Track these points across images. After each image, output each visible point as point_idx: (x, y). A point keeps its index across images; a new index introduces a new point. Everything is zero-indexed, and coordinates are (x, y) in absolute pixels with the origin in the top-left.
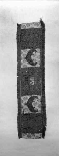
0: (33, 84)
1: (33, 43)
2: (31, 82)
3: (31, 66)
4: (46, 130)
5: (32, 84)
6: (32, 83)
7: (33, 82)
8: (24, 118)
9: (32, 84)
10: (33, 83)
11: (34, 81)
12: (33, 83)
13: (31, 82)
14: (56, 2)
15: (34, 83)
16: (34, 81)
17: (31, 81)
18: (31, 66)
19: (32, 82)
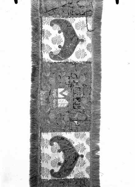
0: (60, 90)
5: (64, 91)
7: (60, 96)
9: (64, 91)
10: (61, 93)
11: (57, 98)
12: (61, 93)
13: (66, 96)
16: (57, 98)
17: (65, 97)
19: (64, 95)
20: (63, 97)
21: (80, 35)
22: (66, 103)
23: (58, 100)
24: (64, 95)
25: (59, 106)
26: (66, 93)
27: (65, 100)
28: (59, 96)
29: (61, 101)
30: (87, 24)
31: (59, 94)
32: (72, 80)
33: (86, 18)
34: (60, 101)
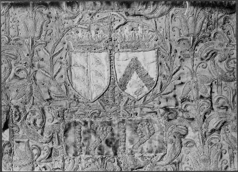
0: (148, 60)
1: (110, 102)
2: (131, 90)
3: (3, 145)
4: (105, 143)
5: (144, 76)
6: (135, 76)
7: (123, 61)
8: (134, 100)
9: (144, 76)
10: (135, 66)
11: (111, 47)
12: (135, 66)
13: (123, 86)
14: (1, 6)
15: (136, 46)
16: (111, 47)
17: (116, 85)
18: (3, 145)
19: (127, 76)
20: (119, 76)
21: (225, 29)
22: (92, 88)
23: (104, 56)
24: (127, 76)
25: (78, 58)
26: (134, 87)
27: (105, 84)
28: (123, 55)
29: (99, 68)
30: (158, 79)
31: (131, 55)
32: (193, 110)
33: (216, 130)
34: (98, 62)
